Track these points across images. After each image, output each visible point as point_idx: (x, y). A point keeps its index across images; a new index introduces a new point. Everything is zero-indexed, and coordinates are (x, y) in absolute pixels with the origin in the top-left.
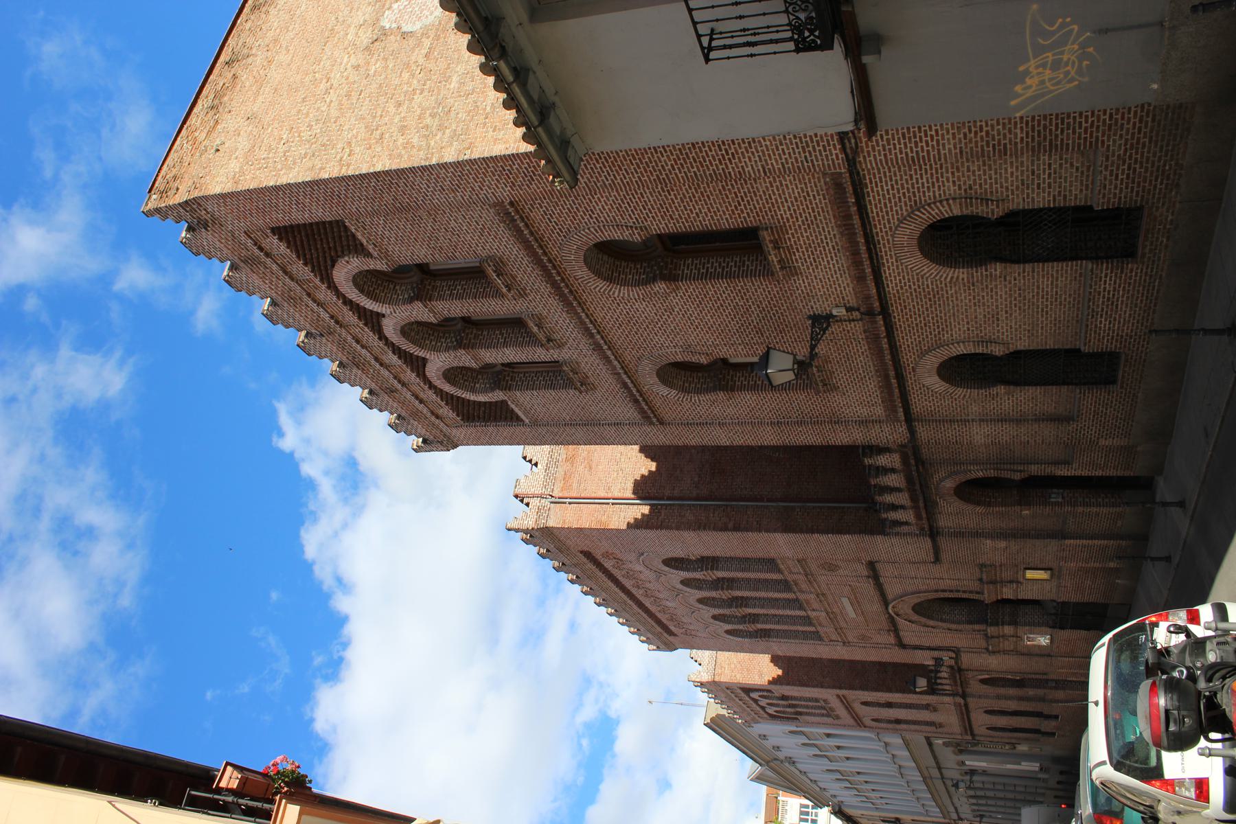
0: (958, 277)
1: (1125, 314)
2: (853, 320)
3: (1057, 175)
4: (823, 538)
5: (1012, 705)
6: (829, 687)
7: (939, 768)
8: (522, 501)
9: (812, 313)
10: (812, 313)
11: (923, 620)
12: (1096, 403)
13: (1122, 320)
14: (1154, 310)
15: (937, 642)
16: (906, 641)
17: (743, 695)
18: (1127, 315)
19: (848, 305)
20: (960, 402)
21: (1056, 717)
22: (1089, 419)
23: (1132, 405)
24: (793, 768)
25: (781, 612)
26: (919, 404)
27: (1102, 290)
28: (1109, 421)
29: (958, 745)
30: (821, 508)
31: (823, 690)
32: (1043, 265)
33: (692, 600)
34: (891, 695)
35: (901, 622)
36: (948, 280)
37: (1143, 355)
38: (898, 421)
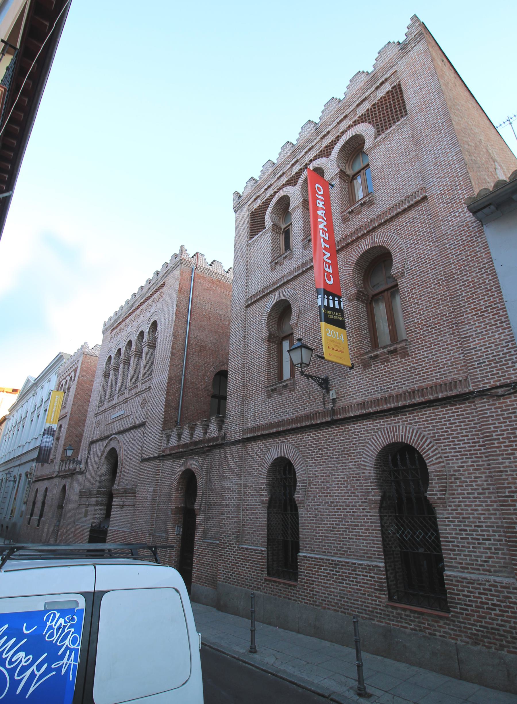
0: (366, 470)
1: (334, 588)
2: (324, 404)
3: (477, 545)
4: (163, 398)
5: (48, 502)
6: (72, 408)
7: (19, 465)
8: (195, 255)
9: (330, 379)
10: (330, 379)
11: (105, 454)
12: (253, 561)
13: (328, 585)
14: (338, 611)
15: (90, 462)
16: (94, 446)
17: (74, 368)
18: (332, 590)
19: (337, 400)
20: (256, 471)
21: (38, 525)
22: (240, 556)
23: (250, 586)
24: (31, 395)
25: (119, 381)
26: (255, 447)
27: (357, 573)
28: (237, 568)
29: (31, 474)
30: (179, 398)
31: (71, 406)
32: (378, 530)
33: (131, 338)
34: (63, 439)
35: (105, 442)
36: (362, 463)
37: (295, 598)
38: (243, 434)
